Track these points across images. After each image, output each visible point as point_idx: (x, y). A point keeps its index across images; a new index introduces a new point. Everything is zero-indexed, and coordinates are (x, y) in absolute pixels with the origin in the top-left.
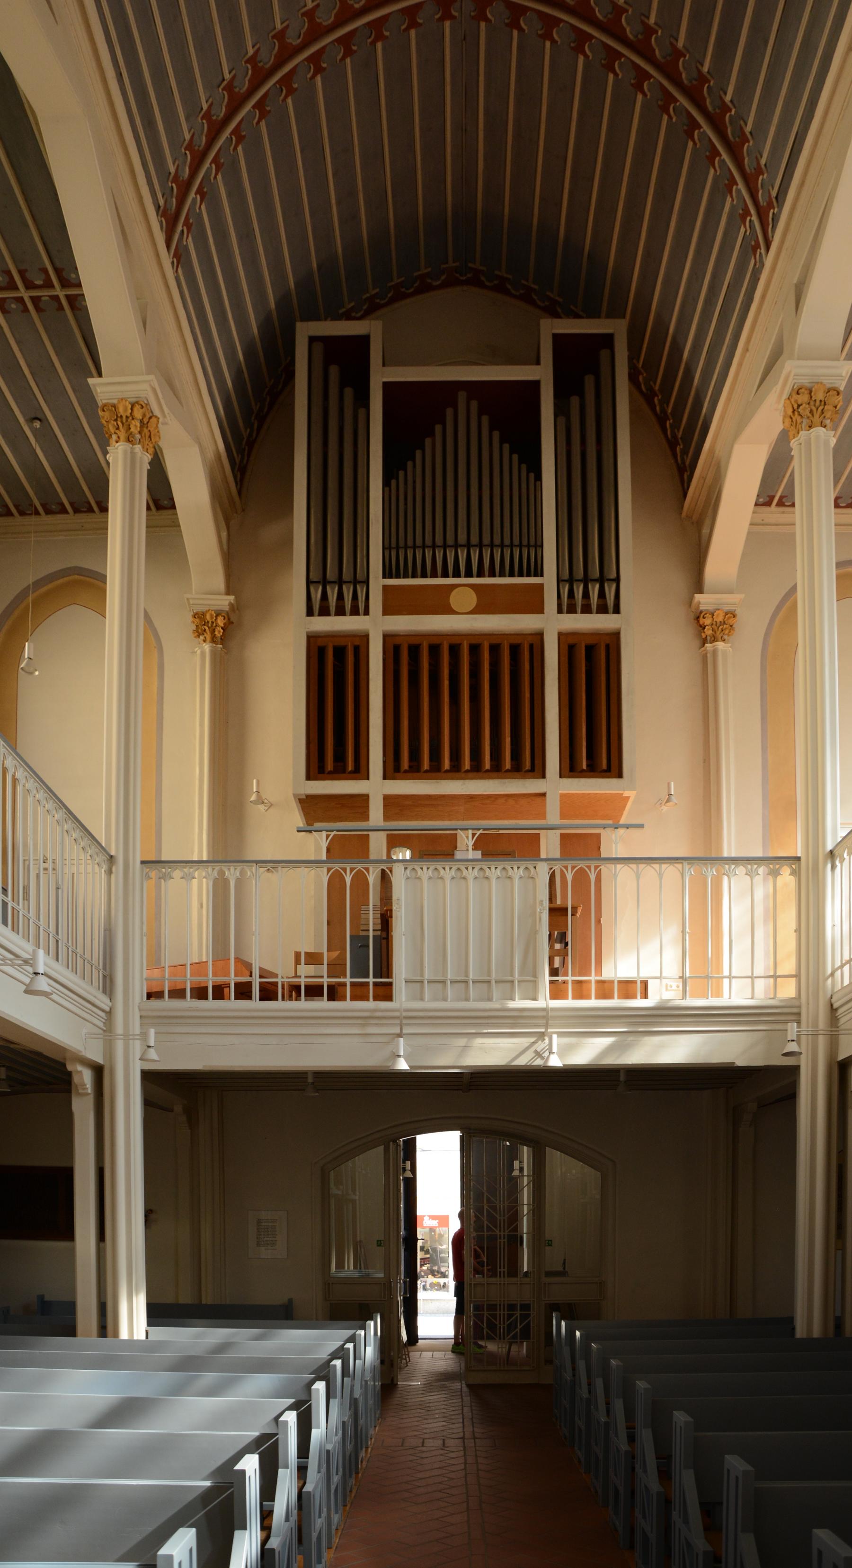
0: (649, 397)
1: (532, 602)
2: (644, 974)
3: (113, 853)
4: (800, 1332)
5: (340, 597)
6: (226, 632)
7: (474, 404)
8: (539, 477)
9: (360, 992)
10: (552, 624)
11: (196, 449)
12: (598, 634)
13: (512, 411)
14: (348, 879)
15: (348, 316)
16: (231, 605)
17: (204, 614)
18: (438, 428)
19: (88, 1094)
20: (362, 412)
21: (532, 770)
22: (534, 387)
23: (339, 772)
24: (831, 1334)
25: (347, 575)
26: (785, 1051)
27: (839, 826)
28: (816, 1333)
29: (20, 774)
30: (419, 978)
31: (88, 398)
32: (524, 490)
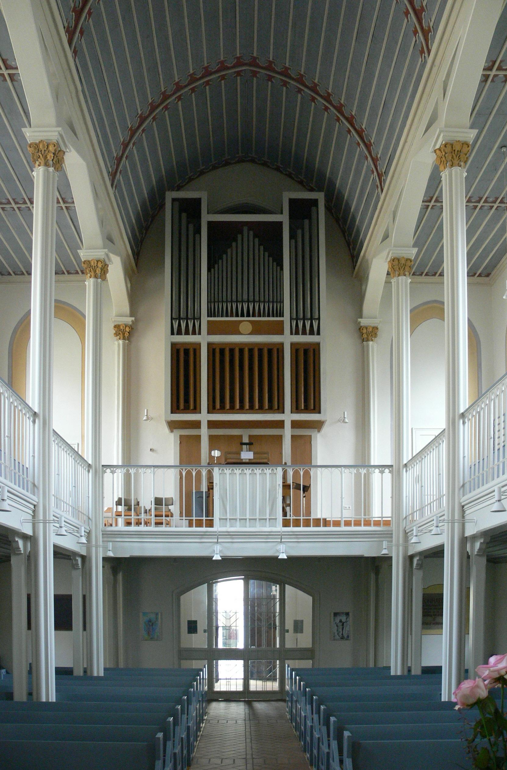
1: (278, 329)
2: (324, 517)
4: (393, 673)
6: (127, 334)
8: (282, 269)
9: (199, 524)
10: (287, 339)
13: (269, 235)
14: (194, 474)
16: (132, 321)
22: (281, 223)
23: (186, 409)
24: (406, 673)
26: (382, 553)
28: (399, 673)
31: (21, 137)
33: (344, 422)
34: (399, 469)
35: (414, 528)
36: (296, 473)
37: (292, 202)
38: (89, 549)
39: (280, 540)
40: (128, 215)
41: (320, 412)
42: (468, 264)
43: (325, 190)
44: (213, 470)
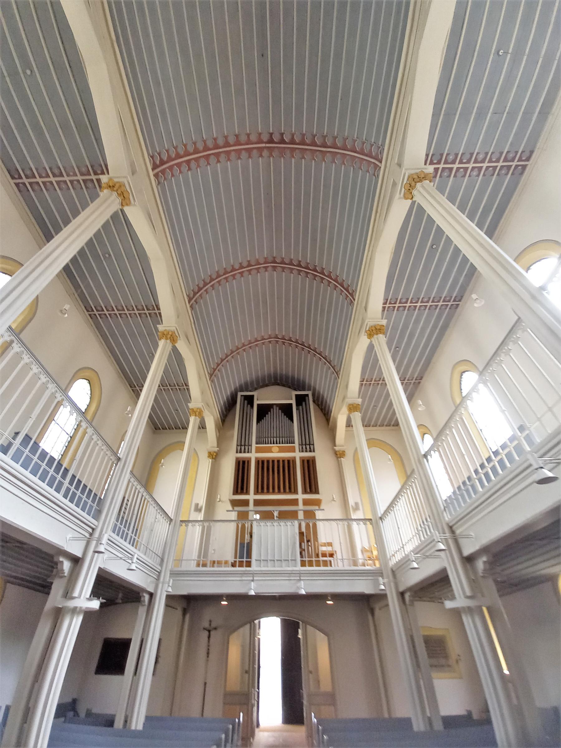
0: (318, 405)
1: (293, 450)
4: (415, 728)
6: (215, 457)
7: (278, 408)
9: (241, 565)
10: (298, 455)
11: (212, 417)
12: (310, 457)
13: (286, 410)
15: (250, 391)
19: (145, 605)
23: (242, 492)
25: (246, 444)
29: (147, 497)
31: (187, 406)
33: (333, 500)
34: (377, 521)
36: (308, 526)
37: (296, 396)
40: (219, 400)
42: (398, 375)
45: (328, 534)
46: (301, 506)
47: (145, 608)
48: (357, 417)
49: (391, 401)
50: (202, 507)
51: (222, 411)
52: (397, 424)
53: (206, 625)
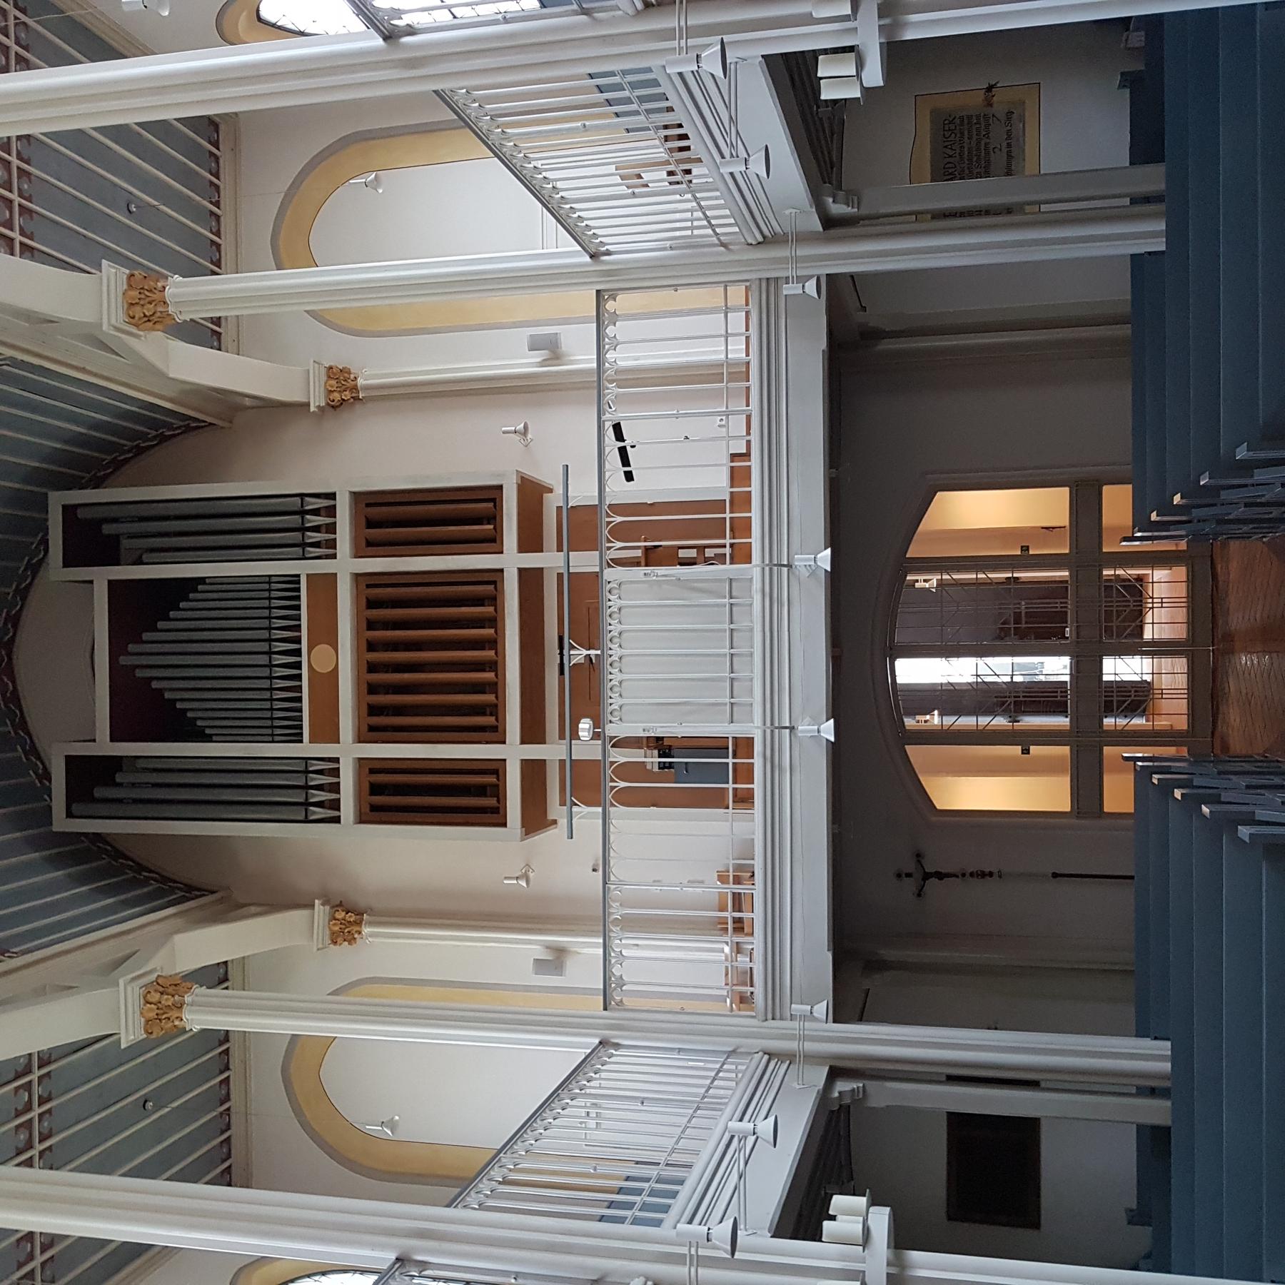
0: (118, 465)
2: (725, 459)
3: (597, 1041)
5: (320, 787)
6: (349, 917)
7: (131, 648)
8: (202, 580)
9: (745, 773)
10: (346, 565)
11: (179, 939)
13: (139, 609)
14: (623, 784)
16: (323, 904)
17: (333, 933)
18: (155, 685)
20: (141, 764)
21: (494, 583)
23: (497, 791)
26: (816, 295)
27: (545, 251)
30: (728, 707)
31: (138, 1049)
32: (215, 596)
35: (725, 170)
36: (620, 532)
38: (813, 1059)
39: (785, 569)
41: (500, 487)
43: (44, 490)
44: (612, 738)
45: (681, 460)
46: (549, 560)
47: (872, 1086)
48: (186, 293)
49: (95, 129)
50: (549, 947)
51: (150, 897)
52: (210, 126)
53: (910, 885)
